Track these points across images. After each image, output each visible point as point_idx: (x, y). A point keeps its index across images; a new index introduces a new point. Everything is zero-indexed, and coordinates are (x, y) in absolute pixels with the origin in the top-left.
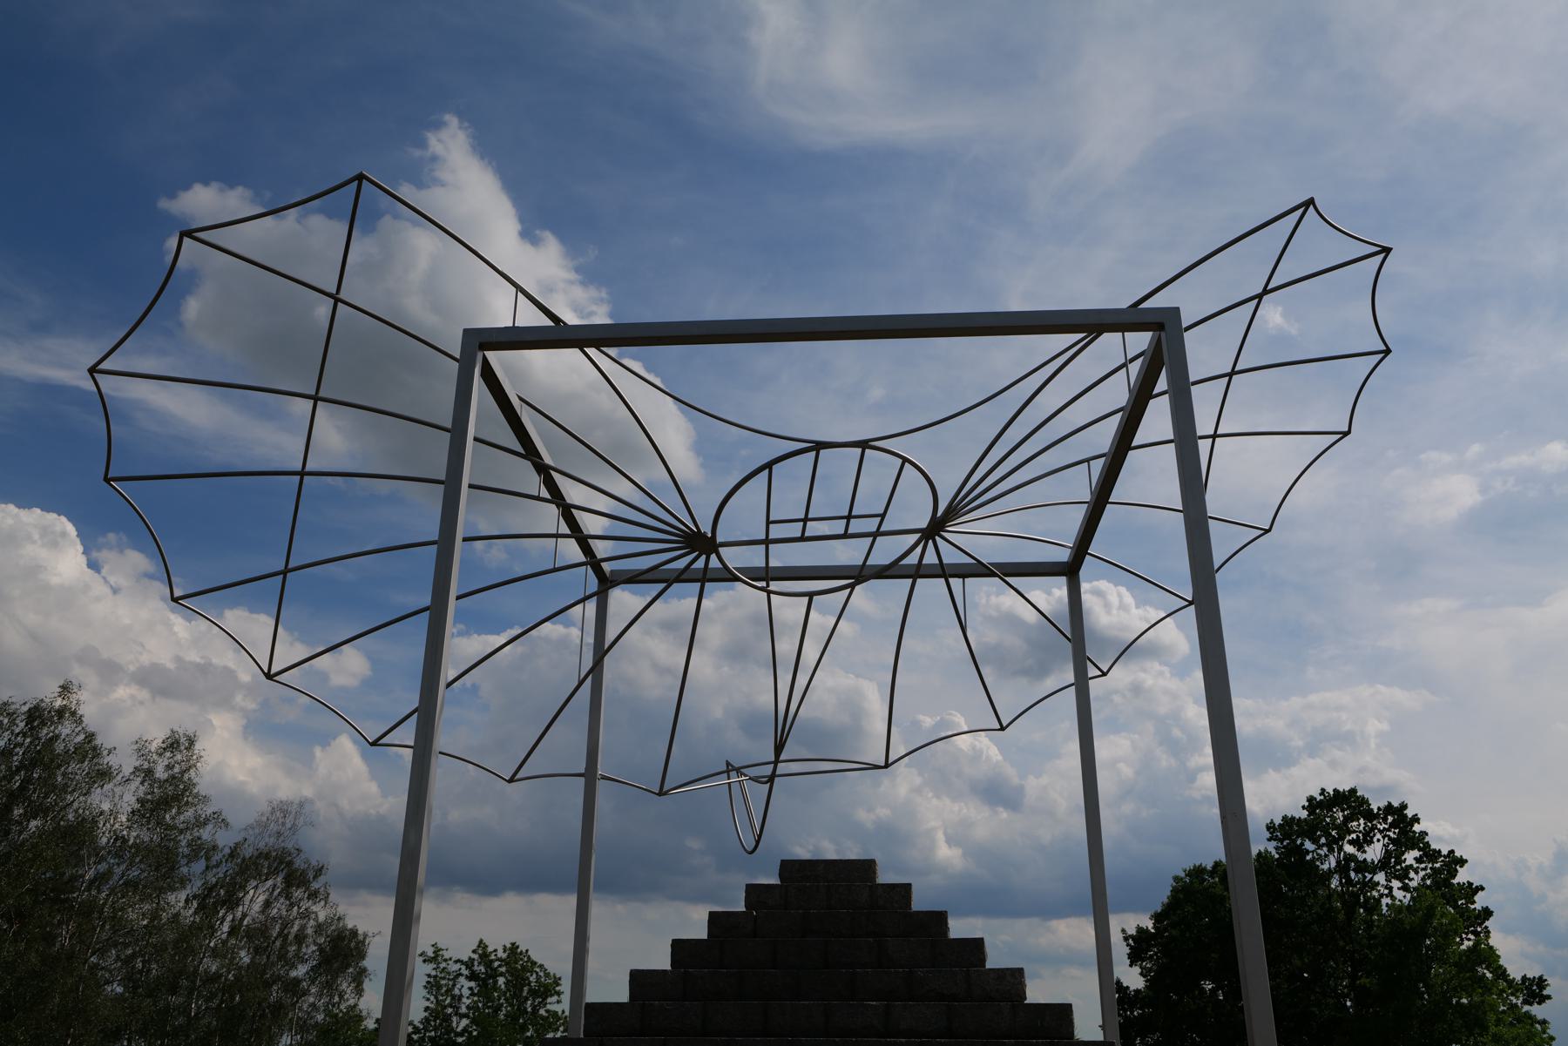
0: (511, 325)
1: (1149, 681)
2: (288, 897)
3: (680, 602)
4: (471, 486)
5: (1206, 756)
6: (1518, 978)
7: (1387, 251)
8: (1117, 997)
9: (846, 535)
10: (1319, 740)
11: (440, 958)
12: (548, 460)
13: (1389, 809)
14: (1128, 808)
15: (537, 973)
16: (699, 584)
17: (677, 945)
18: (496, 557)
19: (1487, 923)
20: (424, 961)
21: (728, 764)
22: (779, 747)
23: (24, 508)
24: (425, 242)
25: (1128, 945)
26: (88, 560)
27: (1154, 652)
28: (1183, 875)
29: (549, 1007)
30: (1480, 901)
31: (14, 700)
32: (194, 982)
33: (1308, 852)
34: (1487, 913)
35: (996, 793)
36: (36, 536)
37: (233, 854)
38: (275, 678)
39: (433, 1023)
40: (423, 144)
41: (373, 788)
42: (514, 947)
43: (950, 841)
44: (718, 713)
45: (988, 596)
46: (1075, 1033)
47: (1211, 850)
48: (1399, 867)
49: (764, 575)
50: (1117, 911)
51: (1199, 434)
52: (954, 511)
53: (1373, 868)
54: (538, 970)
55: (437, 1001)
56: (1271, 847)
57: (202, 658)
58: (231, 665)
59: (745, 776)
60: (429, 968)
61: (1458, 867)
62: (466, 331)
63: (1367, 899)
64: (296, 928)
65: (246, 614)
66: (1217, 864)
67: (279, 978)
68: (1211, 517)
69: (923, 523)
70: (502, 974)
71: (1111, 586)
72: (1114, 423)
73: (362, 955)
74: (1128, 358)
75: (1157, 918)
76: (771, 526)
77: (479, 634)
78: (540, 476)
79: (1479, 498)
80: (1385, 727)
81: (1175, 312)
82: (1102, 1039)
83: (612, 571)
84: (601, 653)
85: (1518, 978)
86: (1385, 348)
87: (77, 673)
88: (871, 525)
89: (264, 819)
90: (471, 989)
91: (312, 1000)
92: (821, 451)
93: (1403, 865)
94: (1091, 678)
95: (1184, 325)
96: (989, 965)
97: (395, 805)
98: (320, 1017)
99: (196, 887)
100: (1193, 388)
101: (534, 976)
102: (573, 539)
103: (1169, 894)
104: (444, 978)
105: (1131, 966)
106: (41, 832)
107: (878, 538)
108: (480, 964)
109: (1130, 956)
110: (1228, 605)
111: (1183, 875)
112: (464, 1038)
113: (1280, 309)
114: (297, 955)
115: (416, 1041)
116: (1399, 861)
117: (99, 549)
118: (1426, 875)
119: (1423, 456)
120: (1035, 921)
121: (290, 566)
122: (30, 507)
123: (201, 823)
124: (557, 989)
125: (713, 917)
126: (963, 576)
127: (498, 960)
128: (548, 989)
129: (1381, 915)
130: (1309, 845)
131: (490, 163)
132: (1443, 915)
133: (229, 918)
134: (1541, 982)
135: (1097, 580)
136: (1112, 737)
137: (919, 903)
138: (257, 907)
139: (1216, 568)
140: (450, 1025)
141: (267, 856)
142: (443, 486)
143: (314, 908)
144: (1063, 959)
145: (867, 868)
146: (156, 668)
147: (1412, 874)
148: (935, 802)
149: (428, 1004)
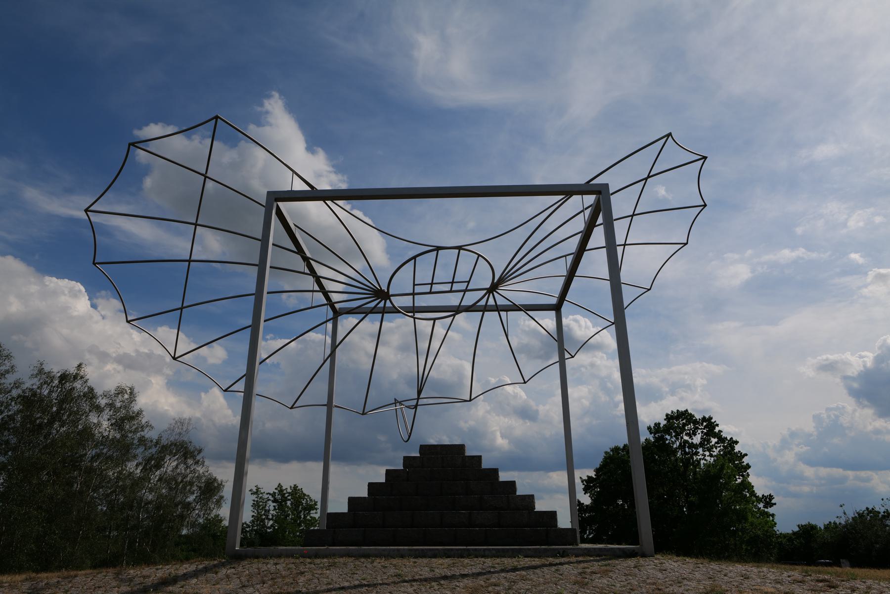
1: (598, 362)
2: (185, 464)
3: (370, 325)
5: (620, 397)
7: (705, 158)
8: (578, 509)
9: (451, 291)
10: (674, 389)
12: (308, 255)
13: (704, 419)
14: (587, 420)
15: (306, 499)
16: (381, 314)
17: (371, 485)
19: (748, 471)
20: (252, 494)
21: (395, 400)
22: (419, 392)
23: (61, 278)
27: (599, 347)
28: (609, 451)
29: (312, 515)
30: (746, 460)
34: (748, 466)
35: (525, 414)
36: (66, 292)
37: (157, 443)
38: (177, 359)
40: (262, 105)
41: (229, 412)
42: (295, 487)
43: (503, 436)
44: (395, 376)
45: (524, 321)
47: (622, 439)
49: (412, 310)
50: (577, 468)
52: (502, 280)
53: (695, 446)
55: (258, 512)
60: (254, 497)
61: (735, 445)
66: (625, 446)
69: (488, 285)
70: (289, 500)
71: (581, 318)
72: (577, 240)
74: (585, 207)
75: (597, 471)
79: (750, 275)
80: (705, 382)
82: (571, 527)
84: (334, 347)
88: (463, 286)
89: (172, 426)
90: (274, 506)
91: (197, 512)
95: (611, 192)
96: (518, 493)
97: (235, 420)
100: (614, 222)
101: (305, 500)
102: (321, 293)
104: (261, 502)
105: (585, 494)
108: (278, 495)
109: (584, 489)
110: (631, 326)
111: (609, 451)
114: (189, 491)
115: (249, 531)
117: (97, 298)
118: (721, 449)
119: (725, 255)
120: (542, 472)
121: (184, 306)
122: (63, 279)
124: (316, 507)
125: (388, 472)
126: (507, 311)
127: (288, 493)
128: (311, 507)
129: (700, 468)
130: (668, 437)
132: (728, 467)
134: (771, 497)
136: (580, 387)
137: (485, 465)
138: (170, 469)
139: (625, 307)
140: (264, 524)
142: (257, 267)
144: (552, 491)
147: (714, 449)
148: (497, 418)
149: (253, 514)
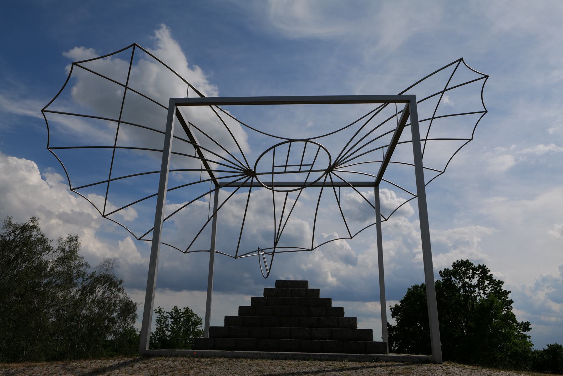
0: (186, 97)
1: (400, 223)
4: (172, 153)
5: (420, 248)
6: (520, 323)
7: (487, 77)
9: (299, 172)
10: (457, 244)
12: (198, 144)
17: (241, 308)
18: (179, 177)
21: (259, 248)
22: (276, 243)
25: (392, 311)
26: (41, 176)
27: (403, 213)
28: (411, 288)
29: (198, 328)
35: (348, 260)
37: (92, 276)
39: (159, 333)
40: (154, 35)
41: (138, 255)
43: (333, 276)
44: (255, 232)
46: (373, 339)
47: (421, 280)
50: (388, 300)
51: (421, 139)
52: (336, 164)
53: (474, 287)
56: (441, 279)
57: (80, 210)
59: (264, 252)
60: (157, 315)
66: (423, 285)
67: (107, 318)
76: (274, 168)
78: (196, 150)
79: (514, 163)
80: (480, 240)
81: (414, 97)
84: (216, 210)
85: (520, 323)
87: (38, 215)
88: (308, 168)
93: (484, 285)
96: (345, 316)
99: (80, 287)
105: (392, 318)
108: (175, 313)
110: (429, 198)
111: (411, 288)
113: (448, 97)
117: (45, 173)
119: (496, 149)
120: (360, 303)
126: (339, 186)
128: (198, 322)
131: (177, 41)
137: (322, 295)
138: (100, 294)
143: (119, 294)
145: (305, 283)
146: (64, 214)
149: (157, 327)
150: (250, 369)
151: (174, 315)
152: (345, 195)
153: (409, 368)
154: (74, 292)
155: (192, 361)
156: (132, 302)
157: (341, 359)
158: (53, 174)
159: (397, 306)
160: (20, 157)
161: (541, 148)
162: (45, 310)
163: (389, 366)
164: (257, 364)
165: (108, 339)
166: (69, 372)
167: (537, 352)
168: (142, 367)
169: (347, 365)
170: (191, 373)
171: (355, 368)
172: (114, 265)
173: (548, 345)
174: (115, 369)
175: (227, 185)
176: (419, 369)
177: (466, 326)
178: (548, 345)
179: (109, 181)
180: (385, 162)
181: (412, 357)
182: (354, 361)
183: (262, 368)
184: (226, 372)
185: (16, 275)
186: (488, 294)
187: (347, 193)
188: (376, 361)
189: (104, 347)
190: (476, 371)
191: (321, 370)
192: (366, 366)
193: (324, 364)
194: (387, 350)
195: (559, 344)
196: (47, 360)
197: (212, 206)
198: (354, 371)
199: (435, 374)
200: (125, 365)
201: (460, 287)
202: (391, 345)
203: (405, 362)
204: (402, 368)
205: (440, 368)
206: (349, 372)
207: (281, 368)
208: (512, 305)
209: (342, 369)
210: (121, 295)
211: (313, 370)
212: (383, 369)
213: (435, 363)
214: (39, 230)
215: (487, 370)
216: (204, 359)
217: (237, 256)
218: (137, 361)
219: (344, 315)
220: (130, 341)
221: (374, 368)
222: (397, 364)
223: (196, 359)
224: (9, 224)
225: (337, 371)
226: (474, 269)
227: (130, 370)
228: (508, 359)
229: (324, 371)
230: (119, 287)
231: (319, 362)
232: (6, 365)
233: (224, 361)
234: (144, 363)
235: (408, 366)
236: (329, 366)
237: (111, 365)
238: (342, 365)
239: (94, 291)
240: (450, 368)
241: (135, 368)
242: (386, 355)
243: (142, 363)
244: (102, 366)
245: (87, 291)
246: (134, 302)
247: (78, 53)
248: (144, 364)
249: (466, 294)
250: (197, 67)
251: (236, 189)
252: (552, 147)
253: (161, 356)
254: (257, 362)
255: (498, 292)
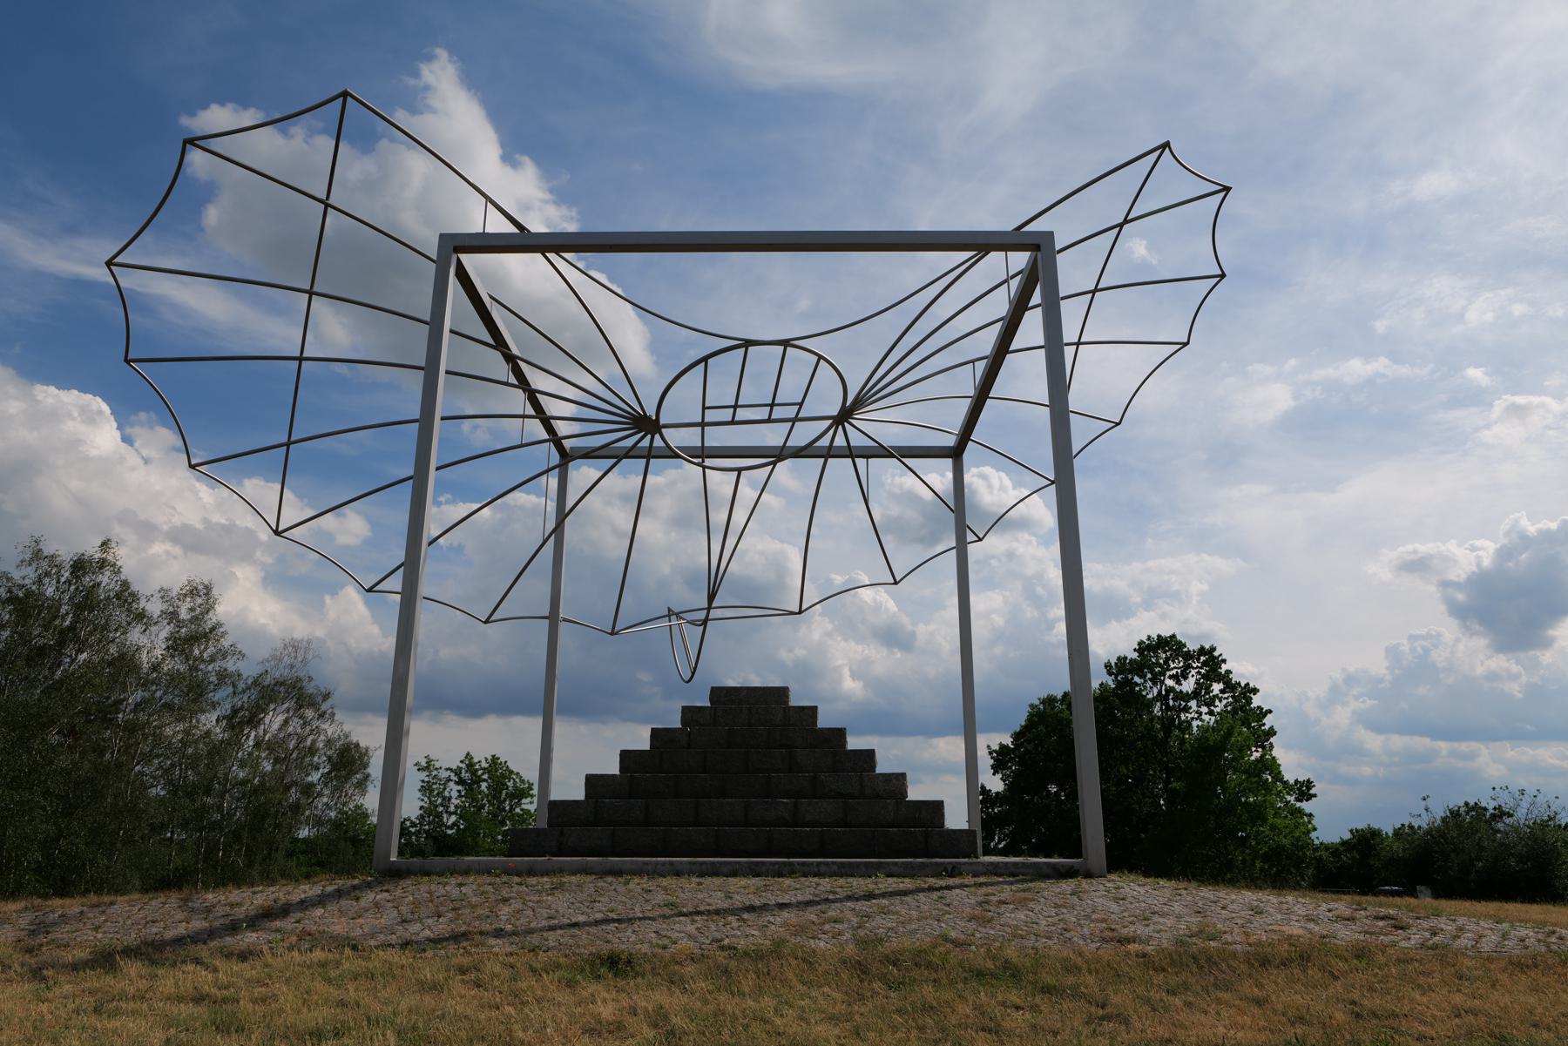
0: (482, 231)
1: (1021, 549)
4: (447, 372)
5: (1059, 611)
6: (1292, 782)
7: (1227, 189)
9: (769, 421)
10: (1152, 598)
11: (431, 767)
12: (515, 351)
13: (1202, 651)
14: (998, 650)
15: (514, 779)
16: (645, 460)
17: (625, 755)
18: (479, 435)
21: (669, 610)
22: (711, 597)
23: (64, 389)
24: (418, 164)
25: (992, 758)
26: (122, 434)
27: (1024, 524)
28: (1037, 702)
29: (523, 806)
30: (1268, 721)
31: (60, 553)
32: (225, 786)
33: (1137, 684)
35: (893, 637)
36: (76, 414)
37: (256, 683)
39: (427, 819)
40: (416, 74)
41: (375, 629)
43: (854, 676)
44: (666, 570)
45: (893, 477)
46: (946, 823)
47: (1059, 683)
48: (1207, 696)
50: (982, 732)
51: (1065, 341)
52: (860, 402)
53: (1186, 697)
54: (515, 777)
55: (430, 801)
56: (1110, 682)
57: (227, 520)
58: (250, 525)
59: (684, 619)
60: (423, 775)
62: (442, 236)
63: (1181, 722)
64: (309, 743)
65: (262, 483)
66: (1066, 695)
67: (295, 783)
68: (1072, 412)
70: (485, 780)
73: (366, 766)
76: (706, 411)
77: (464, 502)
78: (508, 364)
79: (1292, 403)
80: (1205, 587)
81: (1049, 236)
83: (571, 448)
84: (562, 516)
85: (1292, 782)
86: (1221, 273)
87: (117, 531)
88: (791, 412)
89: (278, 653)
90: (459, 791)
92: (750, 348)
93: (1211, 694)
94: (969, 543)
95: (1057, 248)
96: (879, 770)
97: (387, 644)
98: (333, 814)
99: (226, 708)
103: (1377, 828)
105: (994, 774)
106: (87, 663)
107: (797, 423)
108: (467, 771)
110: (1084, 488)
111: (1037, 702)
112: (454, 831)
113: (1144, 242)
116: (1208, 691)
117: (132, 426)
119: (1250, 368)
120: (920, 738)
123: (224, 654)
126: (867, 457)
127: (482, 769)
128: (521, 793)
129: (1191, 734)
130: (1137, 679)
131: (475, 94)
132: (1240, 733)
133: (253, 734)
134: (1309, 784)
135: (983, 466)
136: (989, 593)
137: (823, 722)
138: (276, 726)
140: (441, 820)
141: (282, 684)
142: (423, 372)
143: (323, 726)
145: (782, 693)
146: (186, 528)
148: (843, 644)
149: (422, 804)
150: (647, 901)
151: (465, 775)
152: (889, 481)
153: (1029, 890)
154: (209, 720)
155: (505, 883)
156: (357, 745)
157: (868, 872)
158: (152, 428)
159: (1003, 747)
160: (63, 385)
161: (1357, 368)
162: (138, 768)
163: (981, 885)
164: (665, 889)
165: (300, 836)
166: (196, 917)
167: (1327, 847)
168: (381, 899)
169: (881, 886)
170: (502, 913)
171: (902, 891)
172: (310, 657)
173: (1351, 831)
174: (313, 905)
175: (589, 453)
176: (1052, 892)
177: (1165, 789)
178: (1351, 831)
179: (288, 445)
180: (978, 397)
181: (1035, 863)
182: (898, 876)
183: (677, 897)
184: (588, 907)
185: (61, 681)
186: (1218, 713)
187: (888, 475)
188: (951, 876)
189: (290, 854)
190: (1184, 892)
191: (818, 899)
192: (926, 886)
193: (826, 883)
194: (976, 848)
195: (1376, 826)
196: (145, 890)
197: (552, 506)
198: (897, 900)
199: (1089, 902)
200: (340, 897)
201: (1155, 699)
202: (988, 837)
203: (1018, 876)
204: (1011, 890)
205: (1101, 886)
206: (885, 902)
207: (723, 895)
208: (1272, 740)
209: (870, 896)
210: (330, 729)
211: (800, 898)
212: (966, 893)
213: (1089, 875)
214: (118, 572)
215: (1210, 890)
216: (534, 879)
217: (616, 630)
218: (369, 886)
219: (875, 767)
220: (355, 841)
221: (946, 892)
222: (1001, 879)
223: (516, 879)
224: (37, 555)
225: (857, 900)
226: (1188, 656)
227: (351, 908)
228: (1258, 864)
229: (827, 899)
230: (324, 707)
231: (816, 879)
232: (38, 902)
233: (585, 882)
234: (387, 891)
235: (1025, 885)
236: (838, 890)
237: (303, 896)
238: (869, 885)
239: (261, 719)
240: (1123, 888)
241: (363, 903)
242: (975, 860)
243: (381, 891)
244: (281, 900)
245: (242, 720)
246: (362, 744)
247: (217, 117)
248: (386, 894)
249: (1167, 714)
250: (526, 160)
251: (611, 464)
252: (1381, 364)
253: (428, 874)
254: (664, 884)
255: (1242, 708)
